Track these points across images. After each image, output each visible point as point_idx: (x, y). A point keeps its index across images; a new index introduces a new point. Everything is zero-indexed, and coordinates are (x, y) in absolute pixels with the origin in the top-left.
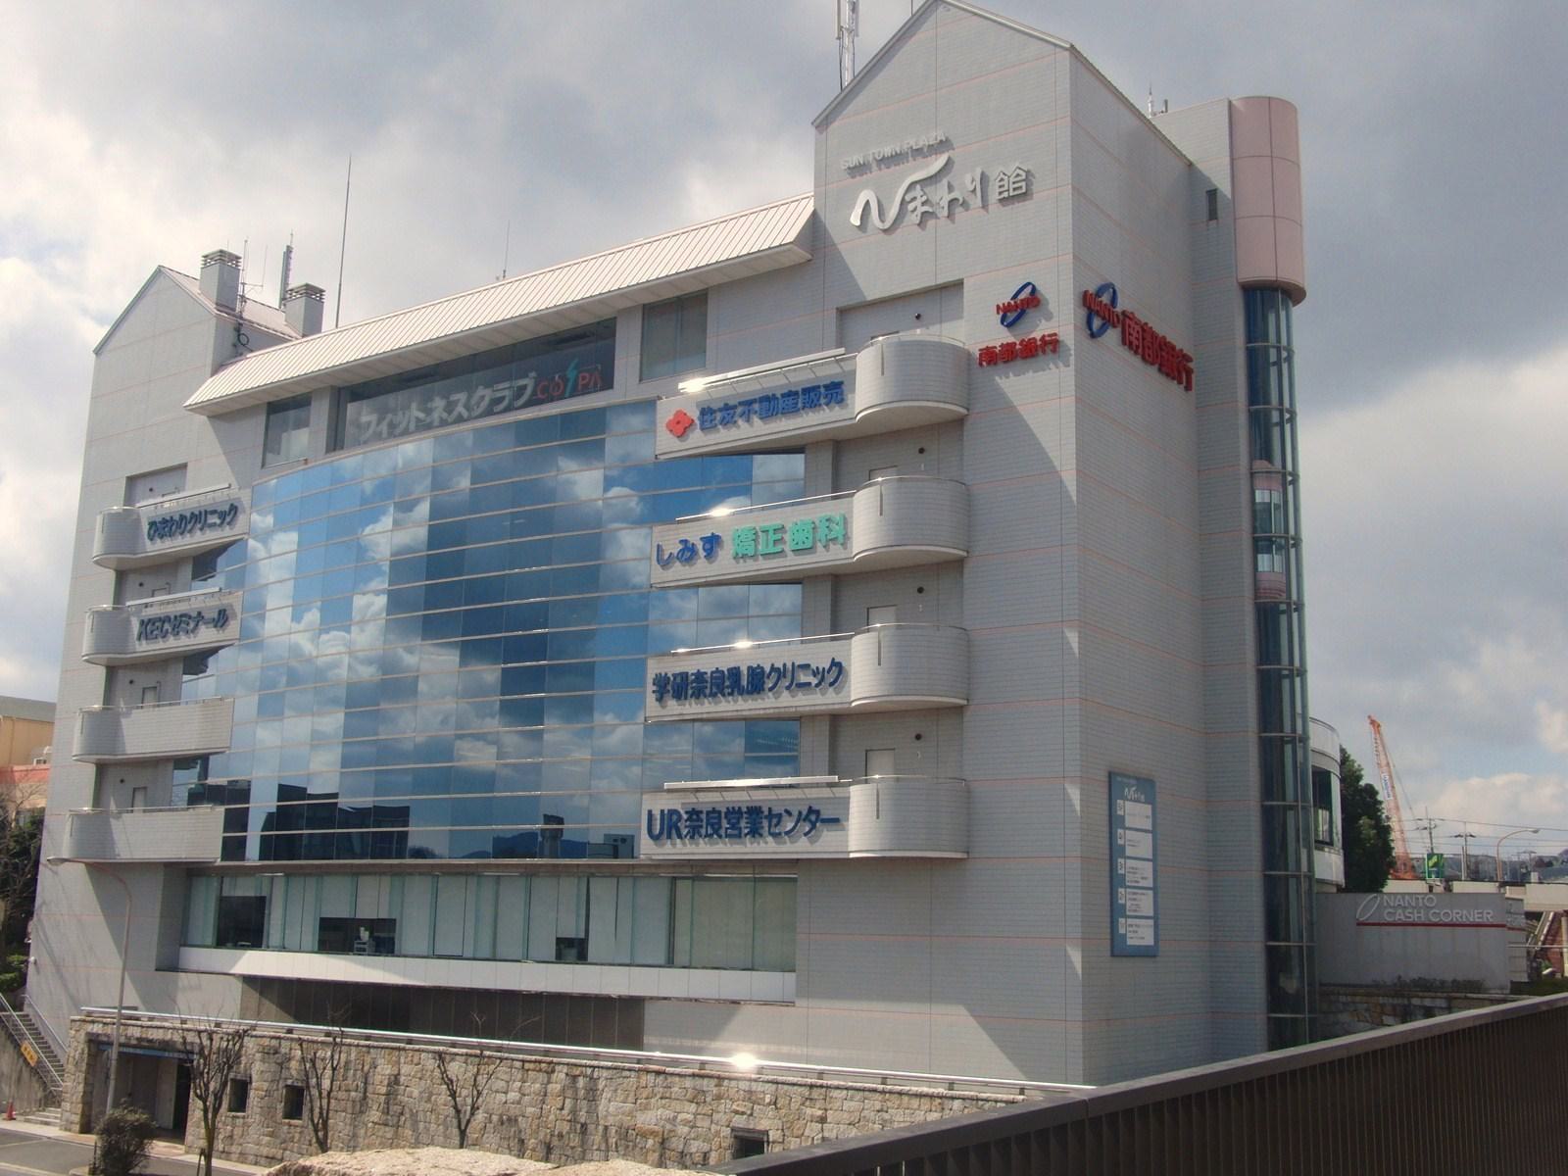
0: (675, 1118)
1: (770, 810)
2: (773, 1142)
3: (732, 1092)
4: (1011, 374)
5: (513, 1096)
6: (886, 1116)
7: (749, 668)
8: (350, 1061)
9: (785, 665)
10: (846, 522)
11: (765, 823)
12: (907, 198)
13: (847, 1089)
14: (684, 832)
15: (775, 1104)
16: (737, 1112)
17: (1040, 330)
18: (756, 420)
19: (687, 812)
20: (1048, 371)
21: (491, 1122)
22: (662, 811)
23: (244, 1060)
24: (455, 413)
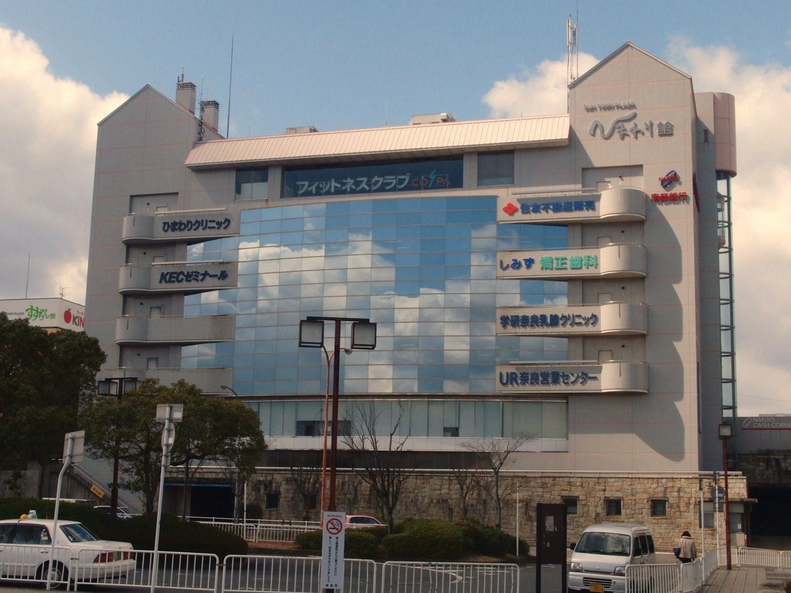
0: (532, 495)
1: (563, 373)
2: (582, 500)
3: (561, 483)
4: (664, 204)
5: (444, 491)
6: (634, 487)
7: (551, 316)
8: (345, 482)
9: (569, 315)
10: (596, 258)
11: (561, 379)
12: (617, 126)
13: (615, 478)
14: (519, 381)
15: (582, 486)
16: (563, 490)
17: (677, 190)
18: (550, 212)
19: (520, 374)
20: (680, 205)
21: (432, 502)
22: (507, 373)
23: (274, 485)
24: (360, 187)
